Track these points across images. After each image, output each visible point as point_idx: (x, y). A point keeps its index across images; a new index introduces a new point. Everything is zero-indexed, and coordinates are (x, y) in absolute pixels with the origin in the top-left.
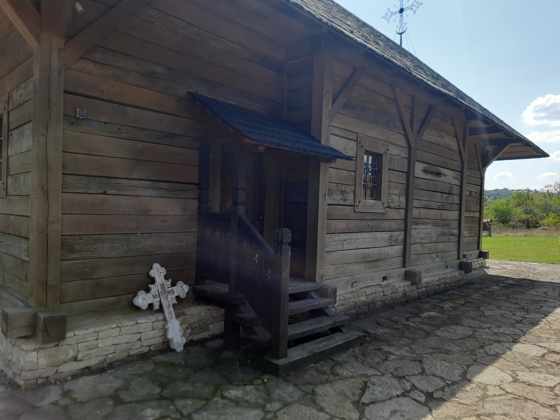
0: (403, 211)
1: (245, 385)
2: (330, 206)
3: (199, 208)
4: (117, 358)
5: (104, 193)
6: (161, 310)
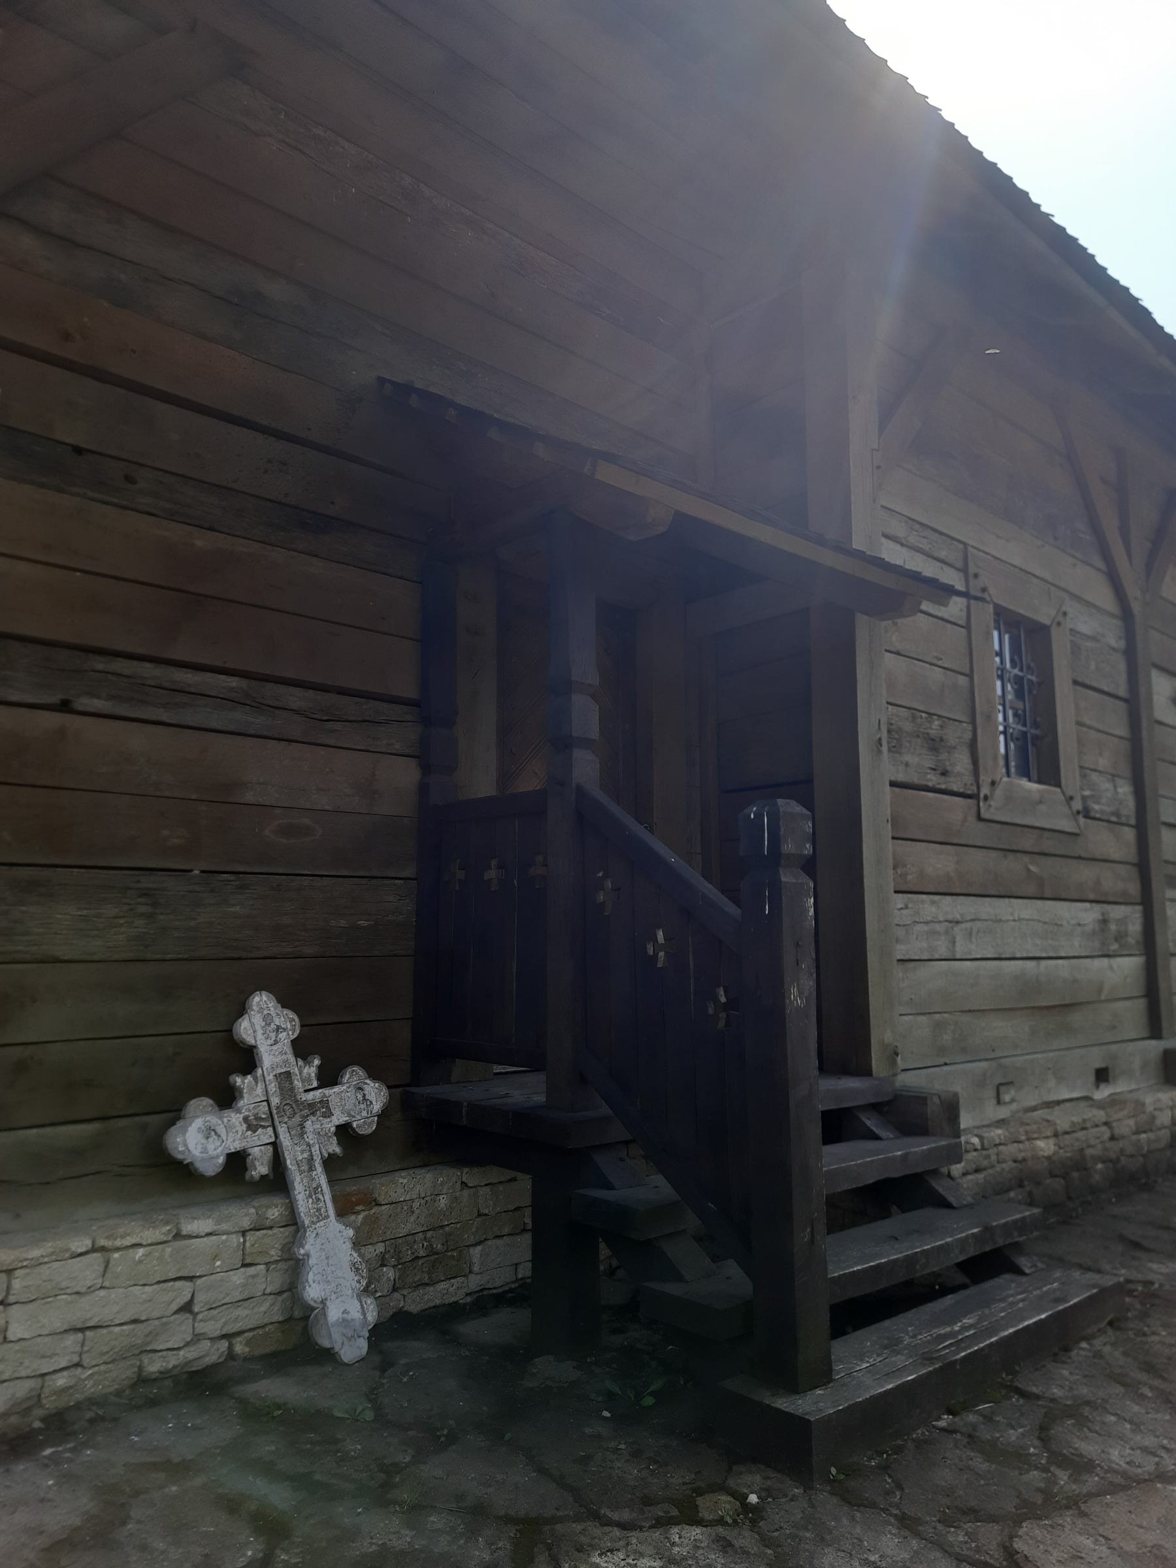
0: (1129, 834)
1: (663, 1523)
2: (897, 790)
3: (423, 789)
4: (91, 1389)
5: (65, 706)
6: (277, 1181)
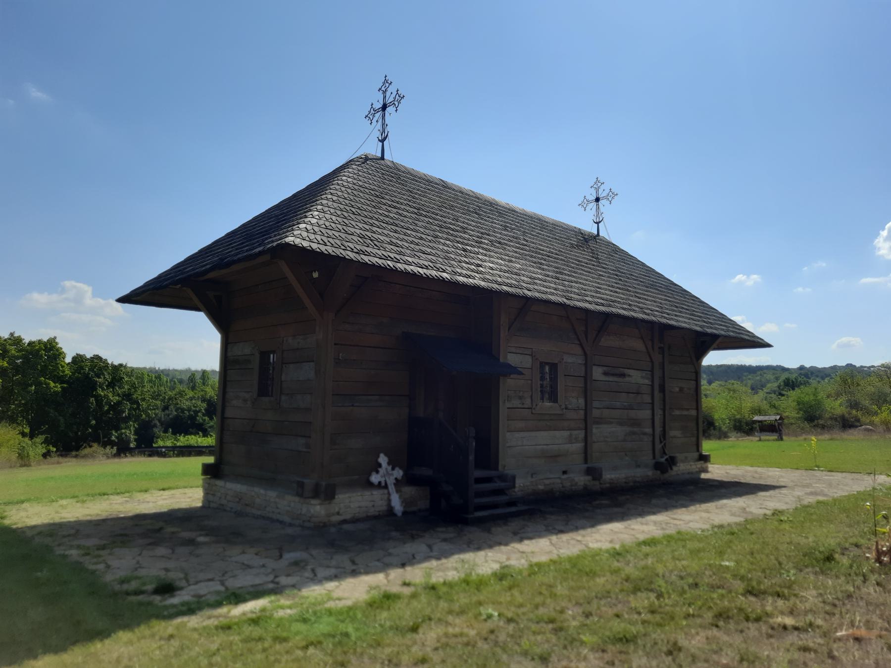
0: (582, 412)
6: (386, 487)
